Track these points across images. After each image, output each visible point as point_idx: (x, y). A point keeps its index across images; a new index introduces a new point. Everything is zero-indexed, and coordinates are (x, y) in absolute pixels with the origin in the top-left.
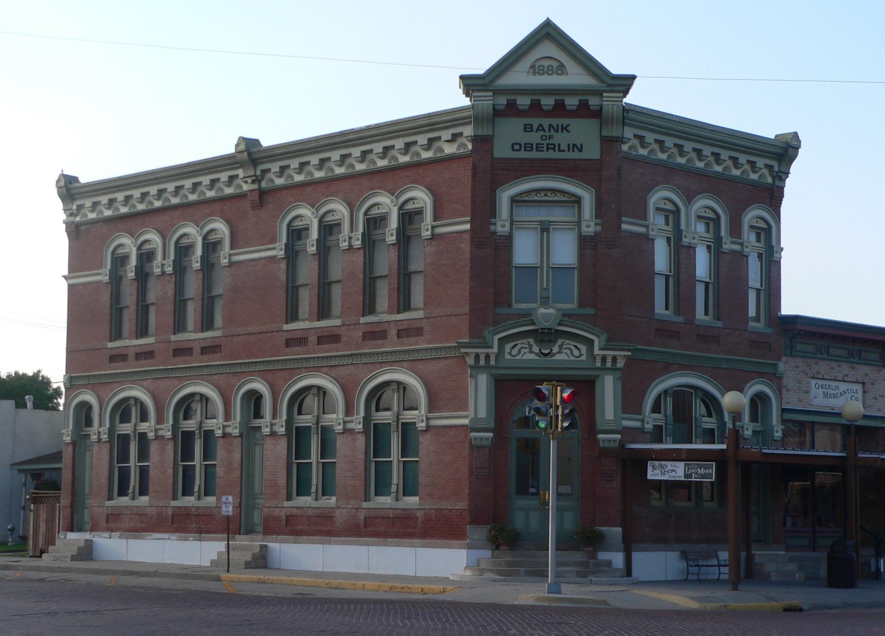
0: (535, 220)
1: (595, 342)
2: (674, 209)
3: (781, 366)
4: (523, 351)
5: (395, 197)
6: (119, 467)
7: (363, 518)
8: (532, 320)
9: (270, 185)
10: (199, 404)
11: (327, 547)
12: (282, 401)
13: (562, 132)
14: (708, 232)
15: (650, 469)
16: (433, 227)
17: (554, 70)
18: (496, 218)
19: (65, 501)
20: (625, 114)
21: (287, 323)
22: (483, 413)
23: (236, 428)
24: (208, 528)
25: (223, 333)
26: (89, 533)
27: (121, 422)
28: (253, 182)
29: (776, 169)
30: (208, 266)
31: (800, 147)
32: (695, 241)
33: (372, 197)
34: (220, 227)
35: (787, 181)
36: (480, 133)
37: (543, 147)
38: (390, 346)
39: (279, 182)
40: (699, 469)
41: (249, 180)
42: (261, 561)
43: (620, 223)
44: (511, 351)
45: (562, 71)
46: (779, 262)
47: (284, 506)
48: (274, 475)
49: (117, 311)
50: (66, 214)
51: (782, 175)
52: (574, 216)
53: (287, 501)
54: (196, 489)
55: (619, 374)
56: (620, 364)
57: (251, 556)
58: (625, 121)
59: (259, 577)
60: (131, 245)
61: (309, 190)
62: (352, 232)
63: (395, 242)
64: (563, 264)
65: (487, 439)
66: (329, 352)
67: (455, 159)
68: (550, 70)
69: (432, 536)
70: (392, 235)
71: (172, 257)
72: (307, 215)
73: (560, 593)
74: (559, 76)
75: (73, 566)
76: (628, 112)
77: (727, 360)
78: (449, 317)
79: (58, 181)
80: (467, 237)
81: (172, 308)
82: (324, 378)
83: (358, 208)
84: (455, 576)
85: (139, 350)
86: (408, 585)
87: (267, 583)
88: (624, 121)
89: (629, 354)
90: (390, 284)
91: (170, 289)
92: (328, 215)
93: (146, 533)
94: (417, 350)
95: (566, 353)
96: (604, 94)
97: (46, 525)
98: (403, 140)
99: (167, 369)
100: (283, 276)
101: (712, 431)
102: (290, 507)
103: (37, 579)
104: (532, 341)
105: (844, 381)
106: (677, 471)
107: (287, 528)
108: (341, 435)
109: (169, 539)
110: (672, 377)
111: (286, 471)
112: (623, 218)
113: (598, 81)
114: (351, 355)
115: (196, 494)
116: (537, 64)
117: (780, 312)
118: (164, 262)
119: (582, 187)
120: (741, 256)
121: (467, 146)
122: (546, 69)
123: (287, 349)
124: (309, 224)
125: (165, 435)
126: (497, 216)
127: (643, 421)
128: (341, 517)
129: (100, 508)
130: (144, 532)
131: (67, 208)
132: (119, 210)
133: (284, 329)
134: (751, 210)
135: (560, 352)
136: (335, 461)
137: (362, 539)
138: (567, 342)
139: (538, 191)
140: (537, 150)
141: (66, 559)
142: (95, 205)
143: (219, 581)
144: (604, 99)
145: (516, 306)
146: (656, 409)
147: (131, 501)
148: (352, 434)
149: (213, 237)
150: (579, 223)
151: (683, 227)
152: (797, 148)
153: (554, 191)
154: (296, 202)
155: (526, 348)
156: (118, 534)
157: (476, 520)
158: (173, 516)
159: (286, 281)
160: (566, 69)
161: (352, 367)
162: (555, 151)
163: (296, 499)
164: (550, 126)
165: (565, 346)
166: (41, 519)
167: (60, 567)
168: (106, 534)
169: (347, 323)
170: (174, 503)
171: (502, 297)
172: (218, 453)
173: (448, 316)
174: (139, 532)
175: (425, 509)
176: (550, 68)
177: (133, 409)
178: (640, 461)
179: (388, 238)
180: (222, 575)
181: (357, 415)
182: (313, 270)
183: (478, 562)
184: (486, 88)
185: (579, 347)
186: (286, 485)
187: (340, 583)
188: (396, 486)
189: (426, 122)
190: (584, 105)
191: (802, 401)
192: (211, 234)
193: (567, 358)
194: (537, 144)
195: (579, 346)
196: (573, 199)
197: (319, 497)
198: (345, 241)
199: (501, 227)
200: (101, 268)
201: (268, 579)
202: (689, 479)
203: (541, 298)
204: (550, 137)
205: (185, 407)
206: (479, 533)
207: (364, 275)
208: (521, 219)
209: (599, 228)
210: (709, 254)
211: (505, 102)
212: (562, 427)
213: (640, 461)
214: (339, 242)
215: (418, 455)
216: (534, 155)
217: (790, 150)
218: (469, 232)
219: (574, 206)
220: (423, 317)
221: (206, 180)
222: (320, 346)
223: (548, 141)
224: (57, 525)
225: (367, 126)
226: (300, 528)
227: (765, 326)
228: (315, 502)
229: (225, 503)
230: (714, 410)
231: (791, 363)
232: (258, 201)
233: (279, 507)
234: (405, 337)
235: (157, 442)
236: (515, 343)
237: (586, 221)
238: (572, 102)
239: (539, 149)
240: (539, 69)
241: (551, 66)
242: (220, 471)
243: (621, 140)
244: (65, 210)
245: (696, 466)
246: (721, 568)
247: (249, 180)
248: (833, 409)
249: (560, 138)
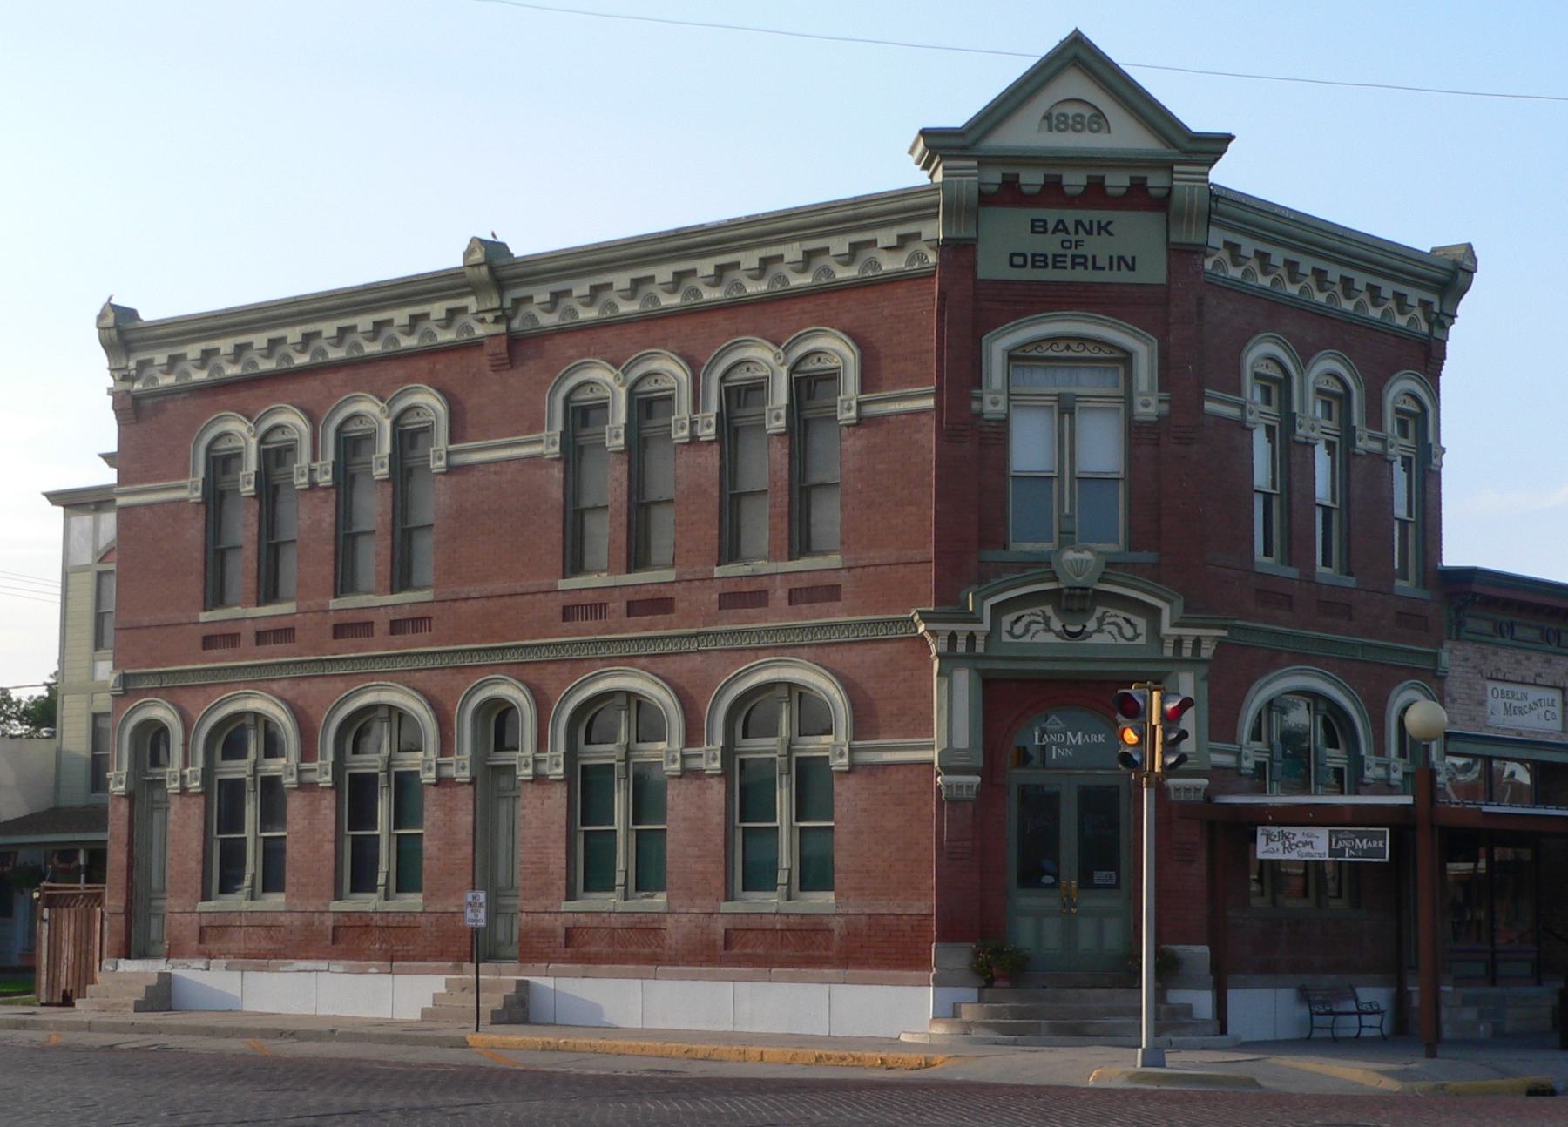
0: (1049, 392)
1: (1163, 612)
2: (1281, 376)
3: (1445, 657)
4: (1034, 628)
5: (783, 349)
6: (221, 839)
7: (723, 932)
8: (1053, 572)
9: (529, 326)
10: (385, 724)
11: (649, 983)
12: (555, 725)
13: (1099, 234)
14: (1330, 418)
15: (1261, 840)
16: (860, 404)
17: (1086, 122)
18: (980, 387)
19: (114, 899)
20: (1213, 204)
21: (564, 577)
22: (962, 741)
23: (463, 768)
24: (408, 951)
25: (297, 608)
26: (164, 961)
27: (224, 758)
28: (497, 320)
29: (1436, 309)
30: (404, 469)
31: (1476, 271)
32: (1314, 434)
33: (736, 348)
34: (429, 401)
35: (1452, 330)
36: (954, 234)
37: (1065, 262)
38: (777, 616)
39: (548, 320)
40: (1357, 840)
41: (489, 317)
42: (519, 1009)
43: (1202, 398)
44: (1012, 628)
45: (1100, 125)
46: (1439, 474)
47: (562, 910)
48: (541, 853)
49: (217, 556)
50: (113, 377)
51: (1445, 319)
52: (1117, 386)
53: (567, 900)
54: (381, 879)
55: (1204, 670)
56: (1207, 653)
57: (502, 1001)
58: (1213, 216)
59: (546, 1039)
60: (616, 386)
61: (607, 335)
62: (696, 410)
63: (784, 430)
64: (1098, 473)
65: (969, 787)
66: (651, 630)
67: (904, 280)
68: (1079, 123)
69: (861, 963)
70: (778, 418)
71: (331, 456)
72: (241, 432)
73: (1163, 1066)
74: (1092, 134)
75: (161, 1022)
76: (1216, 201)
77: (1363, 645)
78: (893, 567)
79: (101, 317)
80: (931, 423)
81: (331, 548)
82: (640, 676)
83: (707, 369)
84: (916, 1035)
85: (263, 626)
86: (853, 1053)
87: (564, 1051)
88: (1209, 218)
89: (1225, 633)
90: (773, 506)
91: (327, 515)
92: (645, 381)
93: (280, 961)
94: (830, 626)
95: (1109, 632)
96: (1176, 168)
97: (74, 946)
98: (801, 246)
99: (322, 661)
100: (556, 493)
101: (1338, 773)
102: (574, 912)
103: (103, 1047)
104: (1049, 610)
105: (1535, 684)
106: (1316, 844)
107: (568, 950)
108: (676, 780)
109: (328, 970)
110: (1281, 676)
111: (564, 845)
112: (1207, 391)
113: (1163, 142)
114: (697, 635)
115: (381, 889)
116: (1055, 113)
117: (1441, 560)
118: (314, 465)
119: (1135, 335)
120: (1383, 460)
121: (926, 257)
122: (1070, 122)
123: (565, 624)
124: (242, 448)
125: (318, 780)
126: (984, 383)
127: (1238, 754)
128: (676, 930)
129: (186, 915)
130: (276, 958)
131: (118, 366)
132: (223, 371)
133: (559, 588)
134: (1397, 380)
135: (1099, 630)
136: (665, 827)
137: (722, 969)
138: (1113, 612)
139: (1053, 340)
140: (1055, 267)
141: (125, 1009)
142: (174, 361)
143: (464, 1047)
144: (1175, 176)
145: (1015, 547)
146: (1256, 735)
147: (249, 902)
148: (699, 779)
149: (412, 422)
150: (1128, 399)
151: (1296, 409)
152: (1471, 272)
153: (1082, 340)
154: (581, 357)
155: (1038, 623)
156: (223, 962)
157: (949, 934)
158: (334, 928)
159: (562, 500)
160: (1107, 121)
161: (699, 658)
162: (1086, 268)
163: (582, 898)
164: (1078, 223)
165: (1108, 620)
166: (65, 937)
167: (133, 1024)
168: (200, 963)
169: (689, 577)
170: (336, 906)
171: (992, 532)
172: (426, 814)
173: (890, 564)
174: (265, 958)
175: (847, 914)
176: (1078, 119)
177: (252, 734)
178: (1244, 825)
179: (770, 422)
180: (469, 1038)
181: (708, 744)
182: (617, 480)
183: (954, 1011)
184: (967, 154)
185: (1132, 621)
186: (565, 871)
187: (715, 1050)
188: (786, 873)
189: (850, 213)
190: (1138, 187)
191: (1474, 720)
192: (409, 414)
193: (1113, 641)
194: (1055, 256)
195: (1134, 619)
196: (1117, 355)
197: (793, 892)
198: (682, 428)
199: (991, 403)
200: (186, 476)
201: (565, 1043)
202: (1339, 859)
203: (1061, 533)
204: (1078, 244)
205: (357, 729)
206: (960, 957)
207: (721, 491)
208: (1025, 391)
209: (1165, 408)
210: (1329, 457)
211: (999, 180)
212: (1163, 765)
213: (1244, 825)
214: (670, 430)
215: (832, 815)
216: (1049, 274)
217: (1461, 275)
218: (934, 413)
219: (1117, 368)
220: (673, 579)
221: (401, 316)
222: (631, 619)
223: (1073, 251)
224: (98, 946)
225: (729, 220)
226: (594, 949)
227: (1417, 585)
228: (623, 901)
229: (470, 904)
230: (1341, 734)
231: (1458, 653)
232: (506, 356)
233: (550, 912)
234: (805, 603)
235: (302, 794)
236: (1020, 613)
237: (1141, 394)
238: (1117, 181)
239: (1058, 264)
240: (1074, 120)
241: (1081, 116)
242: (430, 847)
243: (1202, 250)
244: (112, 370)
245: (1352, 836)
246: (1364, 1017)
247: (489, 317)
248: (1520, 735)
249: (1095, 246)
